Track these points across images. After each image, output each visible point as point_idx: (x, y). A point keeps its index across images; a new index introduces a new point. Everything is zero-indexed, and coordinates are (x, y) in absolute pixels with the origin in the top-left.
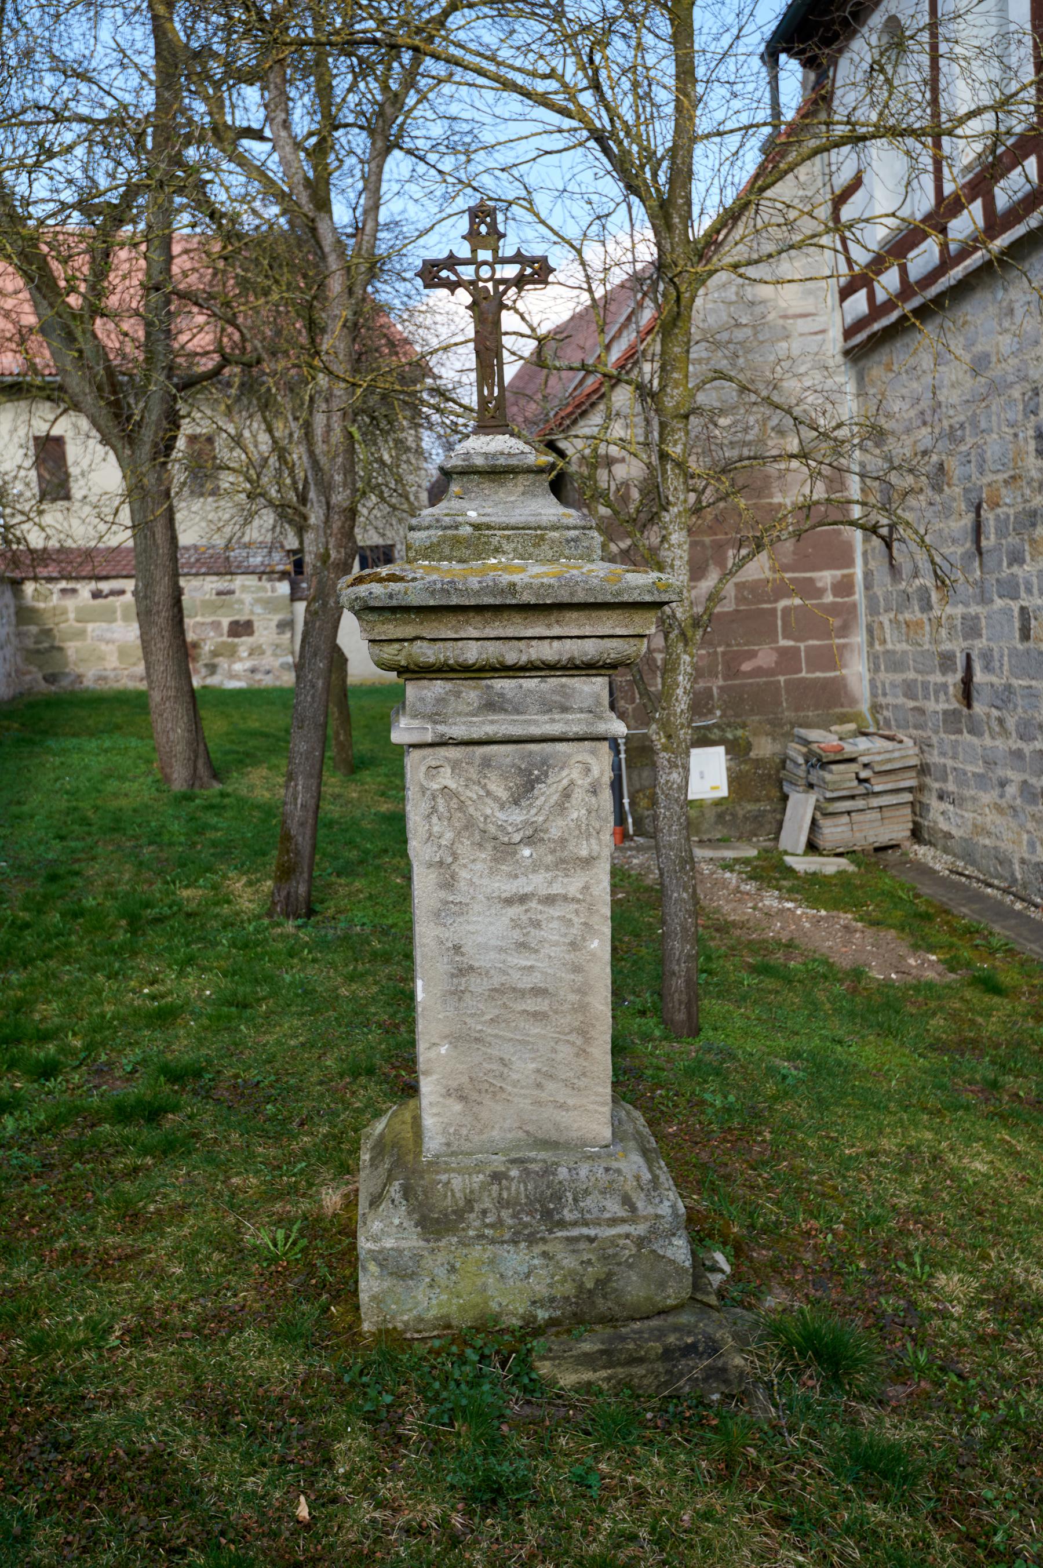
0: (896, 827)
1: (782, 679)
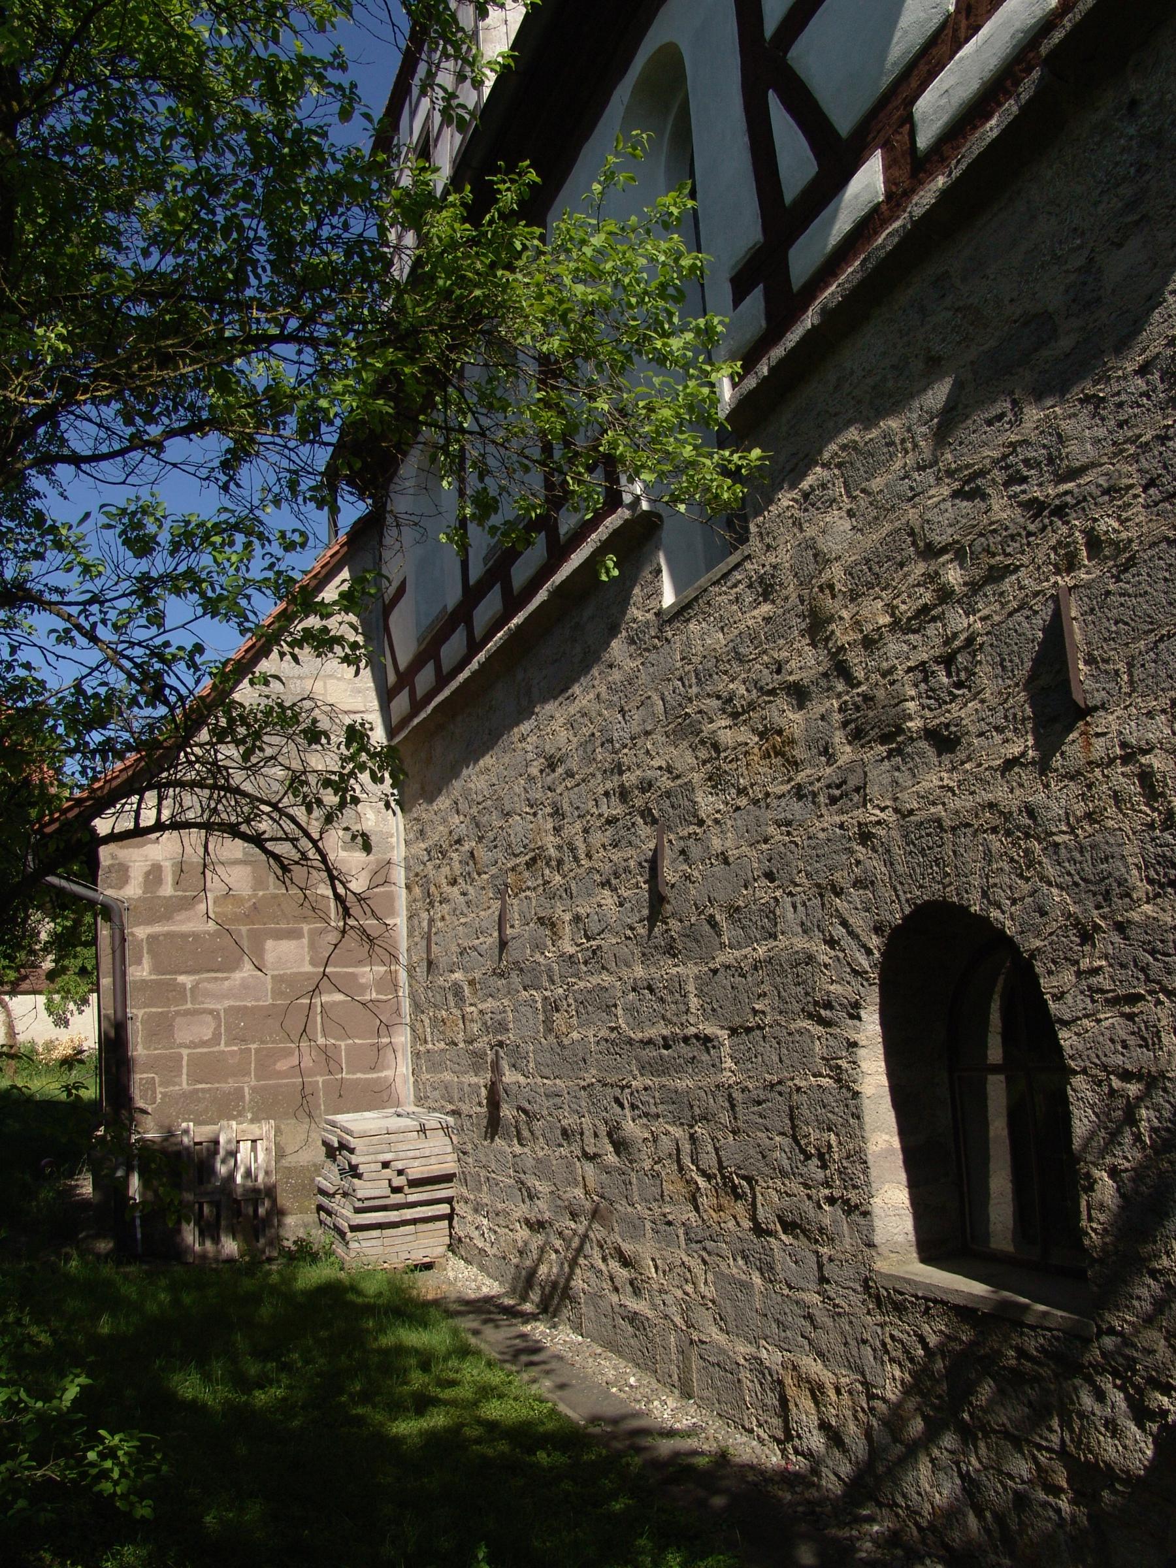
0: (431, 1242)
1: (320, 1079)
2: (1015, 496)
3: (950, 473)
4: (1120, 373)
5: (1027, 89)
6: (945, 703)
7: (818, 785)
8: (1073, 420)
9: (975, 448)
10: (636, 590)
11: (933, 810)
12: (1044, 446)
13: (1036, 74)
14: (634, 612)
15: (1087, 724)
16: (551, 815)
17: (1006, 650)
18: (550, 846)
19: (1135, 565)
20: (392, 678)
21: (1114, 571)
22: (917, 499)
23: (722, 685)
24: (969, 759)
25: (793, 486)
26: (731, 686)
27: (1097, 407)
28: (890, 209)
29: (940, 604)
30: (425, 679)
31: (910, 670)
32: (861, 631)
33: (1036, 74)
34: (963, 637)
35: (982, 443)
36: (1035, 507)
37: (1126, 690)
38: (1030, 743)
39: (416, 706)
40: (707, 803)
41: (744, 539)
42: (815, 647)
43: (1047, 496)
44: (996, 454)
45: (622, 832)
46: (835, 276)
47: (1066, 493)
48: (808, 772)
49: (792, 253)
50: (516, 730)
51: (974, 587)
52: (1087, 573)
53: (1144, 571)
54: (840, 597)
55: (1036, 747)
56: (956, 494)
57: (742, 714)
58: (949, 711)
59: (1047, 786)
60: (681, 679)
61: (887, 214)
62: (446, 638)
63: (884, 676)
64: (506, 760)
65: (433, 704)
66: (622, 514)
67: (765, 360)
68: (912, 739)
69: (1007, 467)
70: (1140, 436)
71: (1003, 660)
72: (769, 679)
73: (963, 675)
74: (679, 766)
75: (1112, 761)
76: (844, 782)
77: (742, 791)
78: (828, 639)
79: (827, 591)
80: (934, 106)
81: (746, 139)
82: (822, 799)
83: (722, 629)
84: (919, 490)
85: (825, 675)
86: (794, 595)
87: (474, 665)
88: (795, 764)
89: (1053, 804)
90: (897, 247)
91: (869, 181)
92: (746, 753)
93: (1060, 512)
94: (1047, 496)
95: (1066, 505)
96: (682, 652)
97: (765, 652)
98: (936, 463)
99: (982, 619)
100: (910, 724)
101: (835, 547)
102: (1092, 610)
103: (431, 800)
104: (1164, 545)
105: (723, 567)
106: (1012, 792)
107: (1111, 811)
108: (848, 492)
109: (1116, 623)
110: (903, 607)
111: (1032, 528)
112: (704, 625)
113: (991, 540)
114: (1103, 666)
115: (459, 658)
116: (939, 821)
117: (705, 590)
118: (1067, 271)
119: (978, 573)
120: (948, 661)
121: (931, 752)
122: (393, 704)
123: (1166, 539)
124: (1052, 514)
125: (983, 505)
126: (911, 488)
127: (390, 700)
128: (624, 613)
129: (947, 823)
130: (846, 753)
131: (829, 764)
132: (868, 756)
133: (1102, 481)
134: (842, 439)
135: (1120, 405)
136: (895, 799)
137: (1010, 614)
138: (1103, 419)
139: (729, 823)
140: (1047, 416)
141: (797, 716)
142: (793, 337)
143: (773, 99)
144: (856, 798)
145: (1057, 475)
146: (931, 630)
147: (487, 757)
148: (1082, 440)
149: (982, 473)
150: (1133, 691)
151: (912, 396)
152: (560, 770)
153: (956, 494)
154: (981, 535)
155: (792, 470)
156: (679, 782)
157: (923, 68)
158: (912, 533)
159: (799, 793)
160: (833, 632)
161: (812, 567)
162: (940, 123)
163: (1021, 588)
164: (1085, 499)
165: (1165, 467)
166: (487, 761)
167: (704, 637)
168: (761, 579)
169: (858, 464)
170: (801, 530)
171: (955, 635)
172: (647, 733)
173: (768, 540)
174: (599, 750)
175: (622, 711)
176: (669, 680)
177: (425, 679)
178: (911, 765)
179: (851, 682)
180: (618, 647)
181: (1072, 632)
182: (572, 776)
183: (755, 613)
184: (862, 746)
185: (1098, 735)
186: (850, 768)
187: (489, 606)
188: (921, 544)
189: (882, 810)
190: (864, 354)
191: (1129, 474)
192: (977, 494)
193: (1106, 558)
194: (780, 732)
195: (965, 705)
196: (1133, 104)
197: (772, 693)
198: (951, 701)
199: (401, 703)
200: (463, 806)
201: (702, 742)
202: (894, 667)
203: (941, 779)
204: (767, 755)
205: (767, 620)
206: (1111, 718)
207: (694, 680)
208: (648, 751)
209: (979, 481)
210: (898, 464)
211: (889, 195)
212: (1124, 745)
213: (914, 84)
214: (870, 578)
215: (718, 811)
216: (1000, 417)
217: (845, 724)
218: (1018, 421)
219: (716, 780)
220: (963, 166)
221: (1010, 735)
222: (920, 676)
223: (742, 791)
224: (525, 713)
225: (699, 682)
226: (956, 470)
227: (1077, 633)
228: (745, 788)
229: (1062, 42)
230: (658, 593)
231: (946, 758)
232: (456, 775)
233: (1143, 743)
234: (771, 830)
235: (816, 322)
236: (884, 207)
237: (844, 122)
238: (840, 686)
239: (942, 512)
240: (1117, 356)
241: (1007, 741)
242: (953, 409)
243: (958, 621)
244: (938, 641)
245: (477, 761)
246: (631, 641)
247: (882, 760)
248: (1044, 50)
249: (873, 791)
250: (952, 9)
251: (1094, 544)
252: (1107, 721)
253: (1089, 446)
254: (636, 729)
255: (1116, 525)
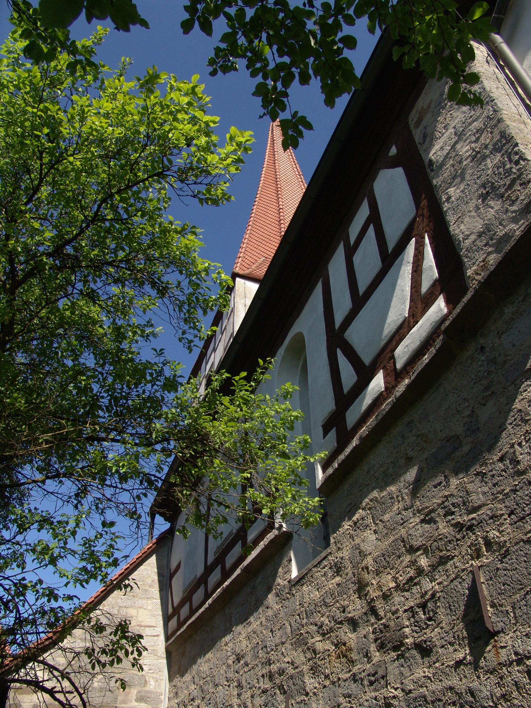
2: (449, 521)
3: (419, 511)
4: (491, 461)
5: (438, 343)
6: (424, 629)
7: (363, 674)
8: (473, 484)
9: (430, 499)
10: (280, 570)
11: (421, 690)
12: (461, 497)
13: (441, 337)
14: (279, 580)
15: (496, 641)
16: (237, 687)
17: (451, 600)
18: (235, 704)
19: (509, 554)
20: (170, 610)
21: (499, 557)
22: (405, 524)
23: (317, 618)
24: (438, 661)
25: (350, 519)
26: (322, 619)
27: (482, 477)
28: (387, 394)
29: (418, 577)
30: (185, 611)
31: (406, 611)
32: (382, 591)
33: (441, 337)
34: (430, 593)
35: (432, 497)
36: (459, 526)
37: (513, 621)
38: (468, 652)
39: (180, 624)
40: (310, 683)
41: (328, 544)
42: (361, 599)
43: (464, 521)
44: (439, 501)
45: (270, 698)
46: (365, 423)
47: (473, 519)
48: (359, 666)
49: (348, 414)
50: (223, 639)
51: (433, 567)
52: (487, 559)
53: (514, 557)
54: (372, 573)
55: (471, 654)
56: (423, 521)
57: (327, 634)
58: (425, 634)
59: (479, 677)
60: (299, 615)
61: (386, 396)
62: (196, 591)
63: (393, 614)
64: (218, 655)
65: (187, 624)
66: (275, 532)
67: (336, 461)
68: (408, 648)
69: (445, 507)
70: (504, 490)
71: (450, 605)
72: (340, 616)
73: (431, 614)
74: (297, 662)
75: (511, 663)
76: (376, 673)
77: (327, 677)
78: (366, 595)
79: (365, 570)
80: (403, 352)
81: (328, 367)
82: (366, 682)
83: (318, 589)
84: (405, 520)
85: (365, 614)
86: (351, 572)
87: (206, 605)
88: (352, 662)
89: (483, 688)
90: (390, 409)
91: (378, 382)
92: (329, 655)
93: (470, 528)
94: (464, 521)
95: (473, 525)
96: (299, 601)
97: (337, 601)
98: (413, 506)
99: (438, 584)
100: (407, 641)
101: (368, 548)
102: (491, 578)
103: (182, 676)
104: (522, 544)
105: (318, 559)
106: (461, 680)
107: (515, 694)
108: (374, 521)
109: (504, 585)
110: (401, 578)
111: (458, 537)
112: (310, 587)
113: (440, 543)
114: (500, 609)
115: (200, 601)
116: (424, 697)
117: (311, 570)
118: (463, 417)
119: (435, 560)
120: (423, 606)
121: (418, 656)
122: (170, 623)
123: (523, 540)
124: (468, 529)
125: (435, 526)
126: (402, 519)
127: (168, 622)
128: (274, 581)
129: (429, 699)
130: (377, 656)
131: (369, 662)
132: (387, 658)
133: (488, 512)
134: (371, 496)
135: (493, 476)
136: (402, 683)
137: (452, 581)
138: (486, 483)
139: (321, 695)
140: (461, 482)
141: (352, 636)
142: (348, 450)
143: (339, 352)
144: (382, 682)
145: (468, 510)
146: (415, 590)
147: (210, 653)
148: (477, 493)
149: (433, 511)
150: (517, 622)
151: (400, 476)
152: (242, 662)
153: (423, 521)
154: (435, 541)
155: (349, 511)
156: (297, 670)
157: (397, 337)
158: (403, 541)
159: (354, 678)
160: (368, 591)
161: (358, 558)
162: (405, 358)
163: (456, 567)
164: (482, 522)
165: (517, 505)
166: (209, 655)
167: (310, 593)
168: (336, 564)
169: (378, 508)
170: (353, 540)
171: (426, 592)
172: (283, 643)
173: (339, 545)
174: (260, 651)
175: (271, 631)
176: (293, 615)
177: (185, 611)
178: (409, 664)
179: (378, 618)
180: (271, 598)
181: (482, 590)
182: (248, 666)
183: (333, 581)
184: (384, 653)
185: (502, 647)
186: (378, 665)
187: (215, 576)
188: (408, 546)
189: (396, 689)
190: (379, 457)
191: (501, 509)
192: (431, 521)
193: (495, 551)
194: (345, 644)
195: (433, 630)
196: (482, 348)
197: (341, 623)
198: (427, 628)
199: (173, 623)
200: (197, 680)
201: (308, 649)
202: (398, 609)
203: (424, 672)
204: (338, 657)
205: (338, 585)
206: (507, 637)
207: (305, 616)
208: (283, 653)
209: (432, 515)
210: (396, 507)
211: (386, 388)
212: (516, 654)
213: (394, 344)
214: (385, 564)
215: (315, 688)
216: (440, 484)
217: (376, 640)
218: (448, 485)
219: (314, 670)
220: (415, 374)
221: (457, 647)
222: (411, 614)
223: (327, 677)
224: (228, 631)
225: (307, 617)
226: (422, 510)
227: (485, 590)
228: (328, 675)
229: (449, 325)
230: (289, 571)
231: (426, 660)
232: (195, 662)
233: (526, 652)
234: (341, 700)
235: (357, 443)
236: (384, 393)
237: (367, 360)
238: (373, 620)
239: (417, 531)
240: (489, 453)
241: (455, 650)
242: (419, 481)
243: (427, 585)
244: (418, 596)
245: (205, 655)
246: (277, 595)
247: (394, 661)
248: (443, 328)
249: (390, 678)
250: (407, 315)
251: (488, 544)
252: (505, 639)
253: (481, 496)
254: (278, 641)
255: (498, 534)
